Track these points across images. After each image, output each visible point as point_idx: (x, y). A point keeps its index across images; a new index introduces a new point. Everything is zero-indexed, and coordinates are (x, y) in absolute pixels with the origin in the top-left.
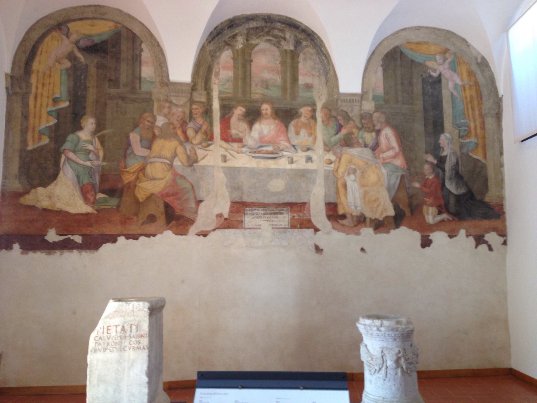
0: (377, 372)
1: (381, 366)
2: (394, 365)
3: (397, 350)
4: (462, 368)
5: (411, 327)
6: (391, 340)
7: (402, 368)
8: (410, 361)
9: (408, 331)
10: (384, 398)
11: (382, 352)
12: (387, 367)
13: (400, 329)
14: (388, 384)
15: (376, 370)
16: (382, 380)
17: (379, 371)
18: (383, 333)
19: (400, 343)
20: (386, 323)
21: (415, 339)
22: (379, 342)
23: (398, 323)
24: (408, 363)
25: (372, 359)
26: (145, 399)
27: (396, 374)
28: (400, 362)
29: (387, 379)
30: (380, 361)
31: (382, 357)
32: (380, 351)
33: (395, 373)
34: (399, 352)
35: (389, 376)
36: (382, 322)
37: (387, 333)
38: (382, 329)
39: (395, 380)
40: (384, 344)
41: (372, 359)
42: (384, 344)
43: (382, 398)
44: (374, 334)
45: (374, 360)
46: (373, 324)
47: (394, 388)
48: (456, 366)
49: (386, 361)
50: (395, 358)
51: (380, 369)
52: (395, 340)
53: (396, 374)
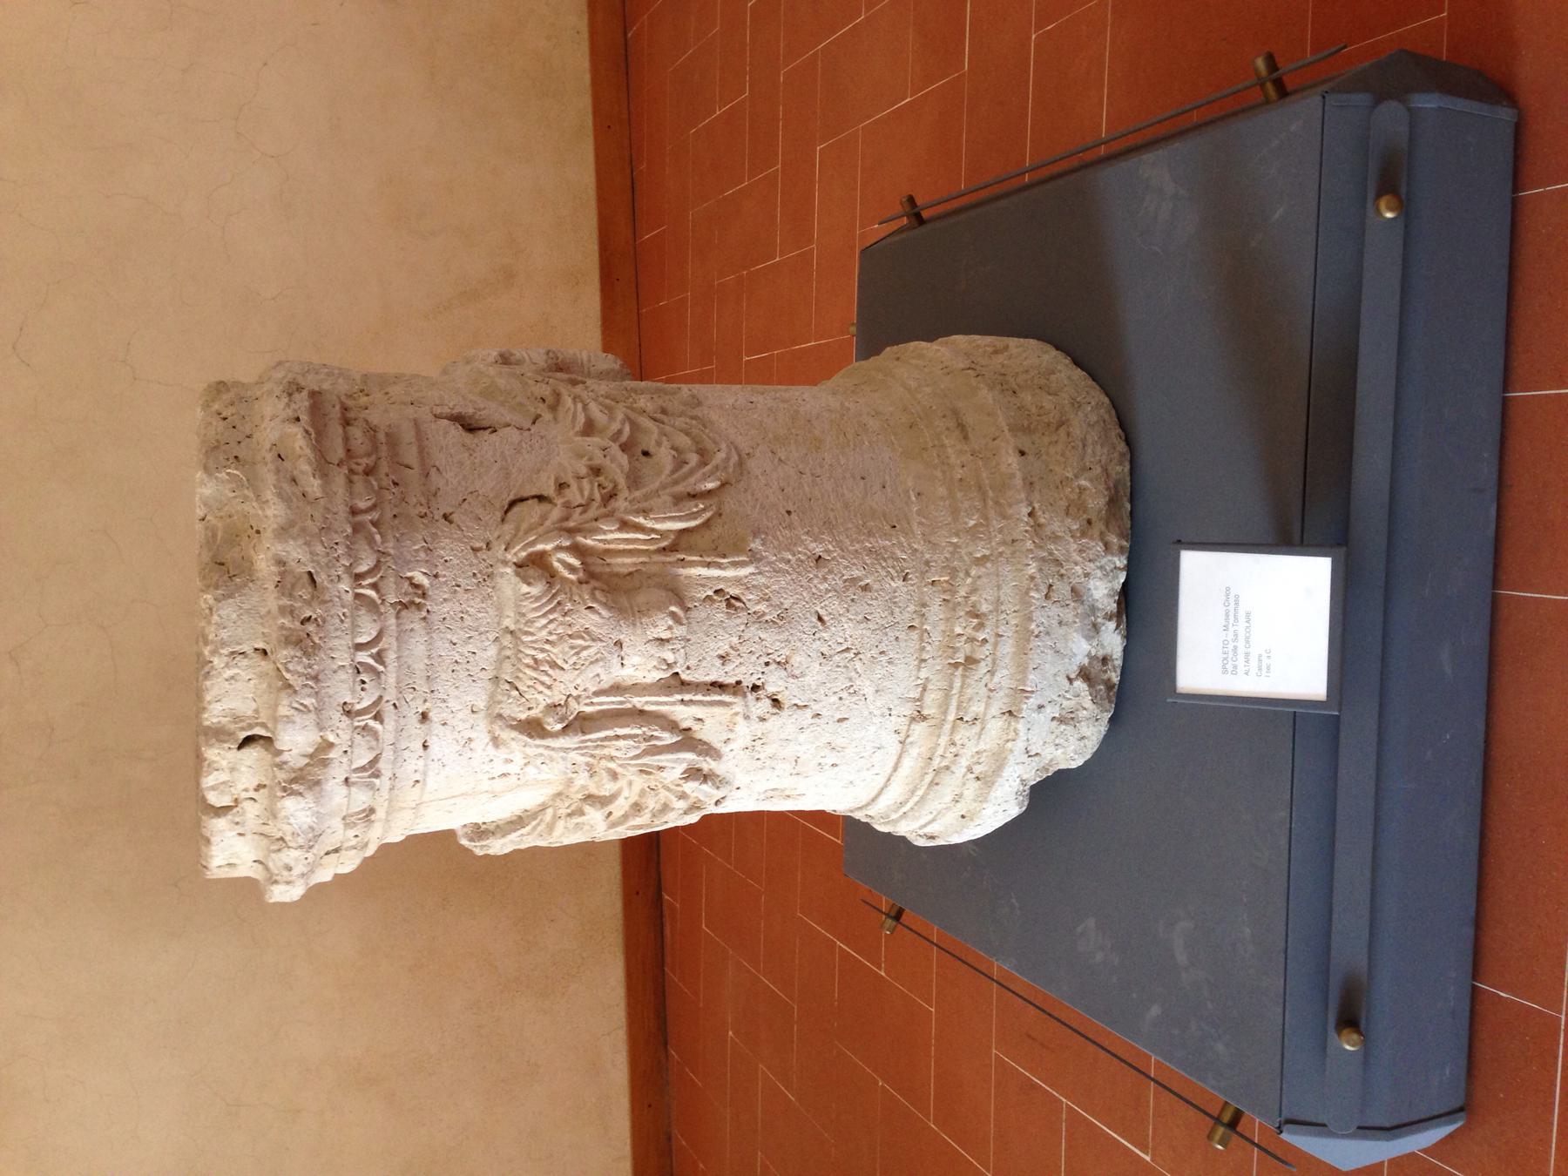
0: (707, 764)
1: (668, 738)
2: (661, 626)
3: (509, 584)
4: (583, 24)
5: (276, 424)
6: (417, 647)
7: (678, 543)
8: (618, 465)
9: (322, 466)
10: (921, 717)
11: (533, 728)
12: (676, 684)
13: (295, 552)
14: (815, 673)
15: (694, 773)
16: (774, 723)
17: (707, 750)
18: (340, 732)
19: (450, 549)
20: (232, 694)
21: (415, 359)
22: (442, 745)
23: (225, 567)
24: (634, 481)
25: (602, 801)
26: (625, 1169)
27: (732, 602)
28: (624, 563)
29: (775, 683)
30: (622, 745)
31: (581, 724)
32: (535, 746)
33: (719, 613)
34: (535, 566)
35: (744, 672)
36: (219, 734)
37: (342, 689)
38: (296, 741)
39: (782, 619)
40: (462, 701)
41: (602, 801)
42: (462, 701)
43: (919, 729)
44: (361, 798)
45: (608, 788)
46: (251, 811)
47: (847, 630)
48: (575, 60)
49: (616, 689)
50: (595, 620)
51: (688, 740)
52: (414, 600)
53: (732, 602)
